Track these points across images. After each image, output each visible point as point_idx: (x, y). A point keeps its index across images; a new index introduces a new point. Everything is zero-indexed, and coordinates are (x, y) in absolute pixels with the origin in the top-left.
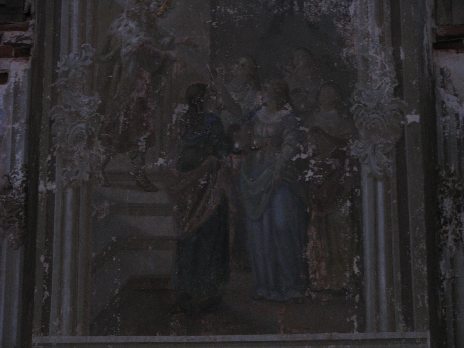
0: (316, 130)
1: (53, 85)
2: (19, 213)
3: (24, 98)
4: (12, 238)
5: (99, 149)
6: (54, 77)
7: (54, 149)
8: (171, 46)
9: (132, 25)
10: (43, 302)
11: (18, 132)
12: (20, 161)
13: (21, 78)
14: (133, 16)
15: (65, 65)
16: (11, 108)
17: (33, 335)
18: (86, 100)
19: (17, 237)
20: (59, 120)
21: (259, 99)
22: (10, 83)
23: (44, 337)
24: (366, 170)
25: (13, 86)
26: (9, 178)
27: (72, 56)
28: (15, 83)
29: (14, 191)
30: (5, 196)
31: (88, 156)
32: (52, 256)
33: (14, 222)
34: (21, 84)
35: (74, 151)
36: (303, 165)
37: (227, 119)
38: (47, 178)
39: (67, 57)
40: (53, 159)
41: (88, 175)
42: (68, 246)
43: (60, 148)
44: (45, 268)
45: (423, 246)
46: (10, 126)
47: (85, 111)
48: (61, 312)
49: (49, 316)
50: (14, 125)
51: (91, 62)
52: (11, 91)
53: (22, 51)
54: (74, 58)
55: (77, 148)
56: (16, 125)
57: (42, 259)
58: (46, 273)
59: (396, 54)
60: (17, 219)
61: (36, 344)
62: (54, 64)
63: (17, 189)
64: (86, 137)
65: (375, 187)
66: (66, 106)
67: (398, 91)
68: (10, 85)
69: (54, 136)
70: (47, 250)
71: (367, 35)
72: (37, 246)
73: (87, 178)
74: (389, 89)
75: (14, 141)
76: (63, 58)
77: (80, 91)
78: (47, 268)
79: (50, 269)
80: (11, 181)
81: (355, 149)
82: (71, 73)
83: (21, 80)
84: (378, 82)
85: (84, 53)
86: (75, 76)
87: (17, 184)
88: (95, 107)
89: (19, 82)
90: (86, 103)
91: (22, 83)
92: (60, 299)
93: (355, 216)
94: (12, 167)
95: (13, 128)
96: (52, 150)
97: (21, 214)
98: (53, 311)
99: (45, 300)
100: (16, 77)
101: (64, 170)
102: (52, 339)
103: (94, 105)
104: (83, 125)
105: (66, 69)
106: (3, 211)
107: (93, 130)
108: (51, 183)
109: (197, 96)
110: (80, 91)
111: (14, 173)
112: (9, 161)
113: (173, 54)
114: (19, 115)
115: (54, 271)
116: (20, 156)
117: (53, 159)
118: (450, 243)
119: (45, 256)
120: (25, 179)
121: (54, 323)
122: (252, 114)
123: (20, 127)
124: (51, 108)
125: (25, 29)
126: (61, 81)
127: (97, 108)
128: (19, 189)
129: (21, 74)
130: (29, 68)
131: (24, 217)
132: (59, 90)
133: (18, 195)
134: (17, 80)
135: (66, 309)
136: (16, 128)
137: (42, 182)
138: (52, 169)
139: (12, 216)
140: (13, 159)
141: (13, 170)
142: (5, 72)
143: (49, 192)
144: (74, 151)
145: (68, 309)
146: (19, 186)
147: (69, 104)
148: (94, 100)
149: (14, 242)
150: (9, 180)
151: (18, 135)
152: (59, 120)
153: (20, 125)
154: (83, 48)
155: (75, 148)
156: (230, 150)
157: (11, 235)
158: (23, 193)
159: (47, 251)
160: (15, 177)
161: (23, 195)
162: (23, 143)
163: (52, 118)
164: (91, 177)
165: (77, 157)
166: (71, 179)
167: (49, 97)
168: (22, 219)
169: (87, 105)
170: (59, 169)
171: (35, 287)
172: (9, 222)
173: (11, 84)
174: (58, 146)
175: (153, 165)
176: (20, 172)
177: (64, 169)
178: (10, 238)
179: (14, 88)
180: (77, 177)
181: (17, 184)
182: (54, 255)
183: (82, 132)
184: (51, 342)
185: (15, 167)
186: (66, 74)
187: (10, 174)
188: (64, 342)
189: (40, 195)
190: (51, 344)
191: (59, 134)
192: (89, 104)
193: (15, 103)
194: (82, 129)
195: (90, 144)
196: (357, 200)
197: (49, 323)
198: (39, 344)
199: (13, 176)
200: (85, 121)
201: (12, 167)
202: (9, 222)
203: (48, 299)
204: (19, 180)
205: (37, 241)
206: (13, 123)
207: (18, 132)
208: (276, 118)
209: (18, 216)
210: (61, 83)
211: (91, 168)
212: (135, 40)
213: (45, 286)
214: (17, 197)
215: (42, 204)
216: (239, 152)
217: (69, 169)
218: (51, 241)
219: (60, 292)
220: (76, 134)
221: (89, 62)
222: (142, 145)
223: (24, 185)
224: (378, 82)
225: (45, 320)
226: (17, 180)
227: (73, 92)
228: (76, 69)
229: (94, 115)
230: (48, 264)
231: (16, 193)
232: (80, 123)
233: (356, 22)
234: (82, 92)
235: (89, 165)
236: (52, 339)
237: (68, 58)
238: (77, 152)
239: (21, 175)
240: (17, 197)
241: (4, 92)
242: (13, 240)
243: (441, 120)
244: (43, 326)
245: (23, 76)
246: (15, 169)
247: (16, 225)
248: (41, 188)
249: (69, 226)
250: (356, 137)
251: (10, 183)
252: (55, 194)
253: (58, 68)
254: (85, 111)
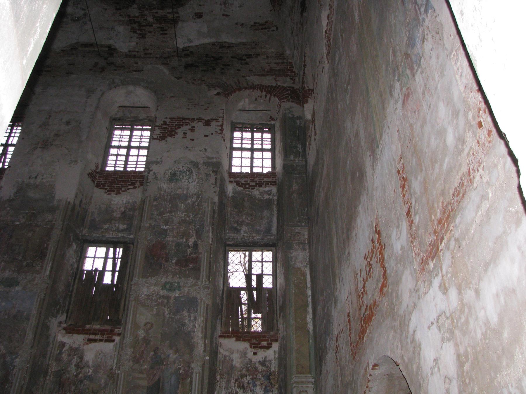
0: (184, 360)
5: (131, 363)
8: (151, 337)
9: (143, 332)
14: (144, 330)
21: (171, 352)
24: (195, 371)
36: (180, 369)
37: (163, 356)
45: (206, 390)
47: (129, 353)
53: (119, 335)
54: (128, 339)
59: (205, 341)
67: (204, 351)
71: (198, 336)
74: (202, 350)
81: (193, 365)
84: (200, 348)
93: (191, 382)
109: (156, 350)
113: (152, 339)
116: (115, 361)
118: (218, 387)
122: (169, 355)
125: (120, 328)
126: (124, 345)
156: (163, 364)
170: (121, 368)
175: (245, 304)
195: (129, 362)
196: (192, 378)
208: (175, 356)
212: (143, 335)
216: (165, 365)
222: (141, 362)
224: (200, 348)
233: (196, 333)
239: (115, 366)
243: (219, 355)
249: (122, 382)
250: (193, 362)
254: (129, 353)
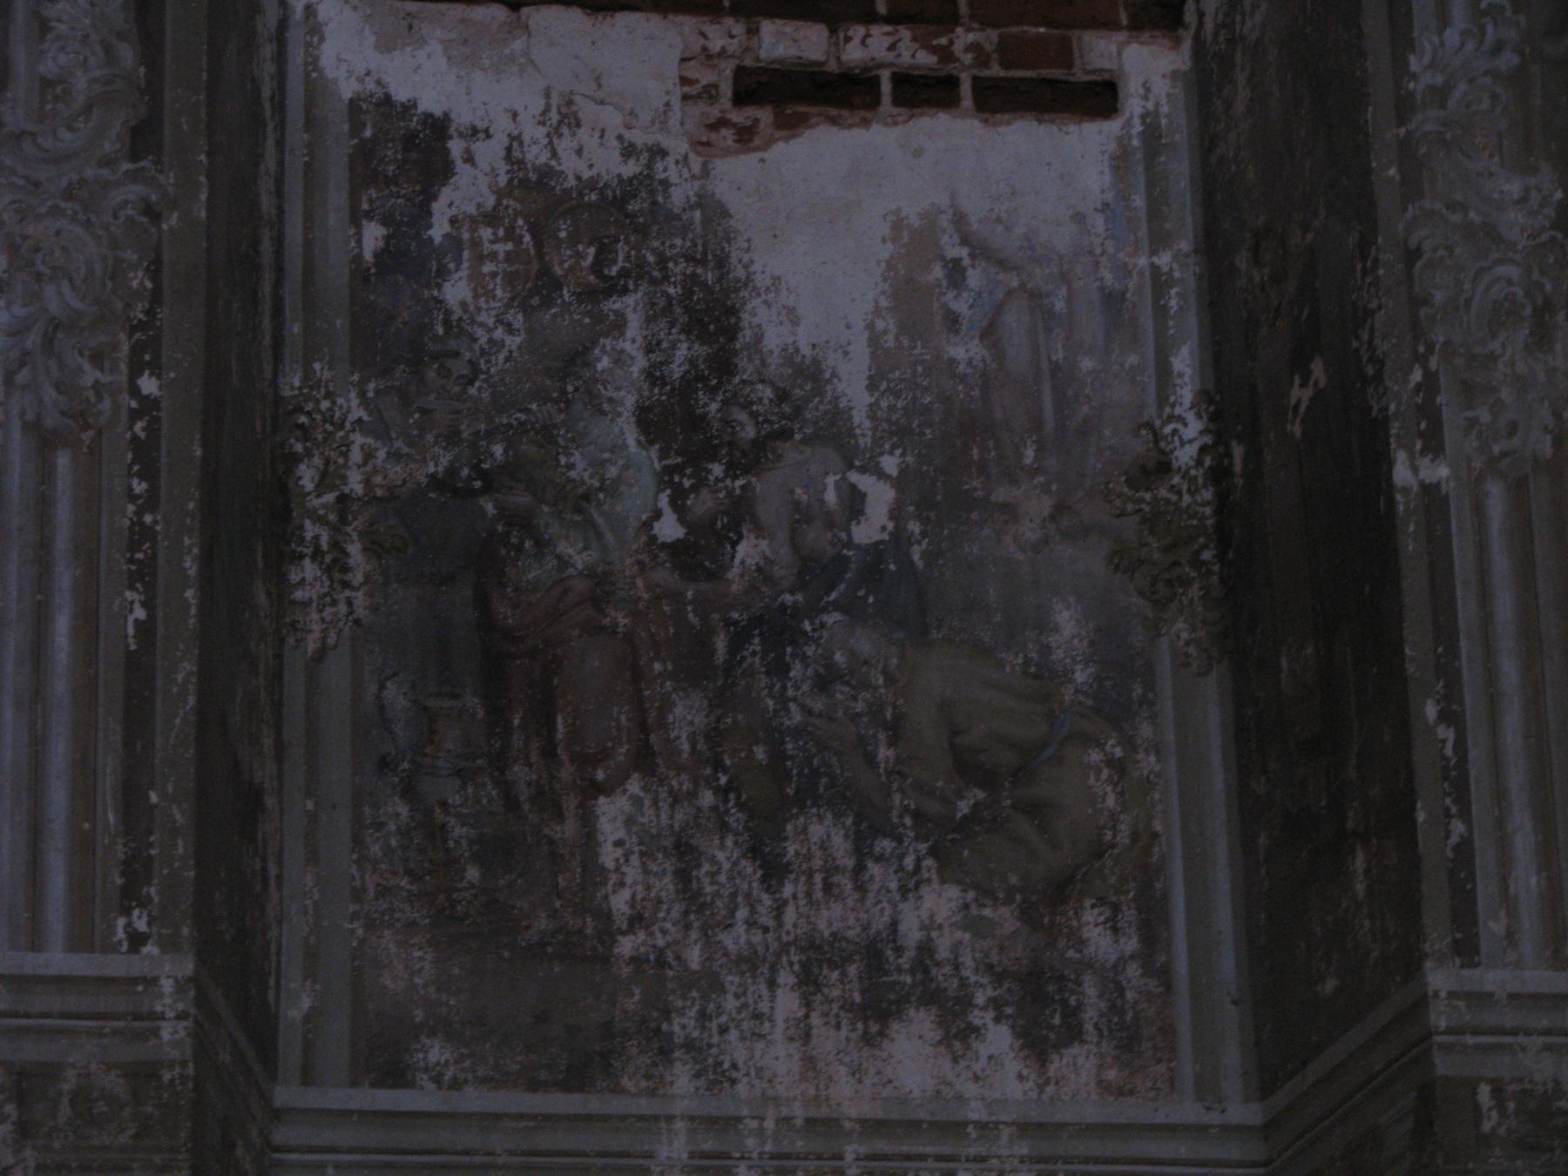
1: (1402, 131)
2: (1198, 553)
3: (1180, 170)
4: (1185, 635)
6: (1404, 108)
7: (1430, 348)
10: (1450, 854)
11: (1171, 283)
12: (1186, 379)
13: (1164, 101)
15: (1432, 65)
16: (1139, 201)
17: (1428, 964)
18: (1514, 187)
19: (1200, 633)
20: (1435, 249)
22: (1127, 114)
23: (1466, 972)
25: (1138, 127)
26: (1157, 436)
27: (1452, 36)
28: (1143, 117)
29: (1176, 480)
30: (1148, 496)
31: (1542, 377)
32: (1461, 703)
33: (1186, 582)
34: (1164, 121)
35: (1493, 357)
38: (1419, 445)
39: (1436, 40)
40: (1430, 380)
41: (1549, 438)
42: (1510, 671)
43: (1447, 343)
44: (1443, 741)
46: (1143, 261)
48: (1512, 890)
49: (1474, 902)
50: (1155, 259)
51: (1516, 60)
52: (1135, 142)
55: (1504, 347)
56: (1164, 260)
57: (1431, 711)
58: (1447, 760)
60: (1194, 574)
61: (1443, 994)
62: (1399, 64)
63: (1187, 472)
64: (1528, 311)
65: (46, 474)
66: (1452, 206)
68: (1128, 124)
69: (1425, 302)
70: (1441, 684)
72: (1411, 669)
73: (1547, 449)
75: (1160, 312)
76: (1426, 44)
77: (1491, 156)
78: (1450, 745)
79: (1460, 744)
80: (1162, 444)
82: (1457, 94)
83: (1165, 109)
85: (1490, 28)
86: (1468, 106)
87: (1185, 456)
88: (1545, 211)
89: (1156, 114)
90: (1515, 197)
91: (1166, 116)
92: (1503, 845)
94: (1162, 400)
95: (1155, 269)
96: (1421, 349)
97: (1206, 555)
98: (1485, 889)
99: (1457, 848)
100: (1146, 98)
101: (1469, 419)
102: (1492, 979)
103: (1541, 206)
104: (1513, 271)
105: (1439, 80)
106: (1146, 545)
107: (1548, 288)
108: (1433, 461)
110: (1491, 156)
111: (1171, 418)
112: (1149, 378)
114: (1167, 226)
115: (1473, 753)
117: (1430, 380)
119: (1438, 702)
120: (1208, 439)
121: (1493, 926)
123: (1175, 266)
124: (1405, 210)
126: (1426, 120)
127: (1553, 214)
128: (1193, 472)
129: (1161, 87)
130: (1185, 68)
131: (1216, 568)
132: (1423, 150)
133: (1189, 490)
134: (1150, 106)
135: (1527, 881)
136: (1165, 269)
137: (1401, 457)
138: (1429, 412)
139: (1176, 563)
140: (1164, 372)
141: (1168, 410)
142: (1106, 76)
143: (1430, 491)
144: (1493, 357)
145: (1533, 880)
146: (1192, 463)
147: (1459, 197)
148: (1539, 190)
149: (1191, 650)
150: (1156, 442)
151: (1173, 292)
152: (1435, 249)
153: (1175, 257)
154: (1484, 13)
155: (1495, 346)
157: (1180, 625)
158: (1205, 485)
159: (1445, 686)
160: (1175, 432)
161: (1208, 494)
162: (1192, 321)
163: (1413, 244)
164: (1557, 443)
165: (1505, 375)
166: (1496, 449)
167: (1392, 171)
168: (1209, 572)
169: (1517, 202)
171: (1419, 805)
172: (1169, 583)
173: (1131, 118)
174: (1441, 339)
176: (1190, 417)
177: (1470, 414)
178: (1178, 637)
179: (1143, 132)
180: (1515, 442)
181: (1185, 456)
182: (1467, 698)
183: (1514, 295)
184: (1489, 988)
185: (1172, 399)
186: (1440, 95)
187: (1158, 422)
188: (1531, 989)
189: (1399, 497)
190: (1491, 995)
191: (1439, 297)
192: (1523, 200)
193: (1150, 184)
194: (1510, 282)
197: (1475, 923)
198: (1452, 995)
199: (1168, 429)
200: (1518, 257)
201: (1162, 400)
202: (1169, 583)
203: (1465, 849)
204: (1191, 441)
205: (1407, 651)
206: (1154, 252)
207: (1171, 283)
209: (1196, 562)
210: (1428, 127)
211: (1557, 415)
213: (1448, 801)
214: (1187, 498)
215: (1411, 529)
217: (1485, 416)
218: (1453, 651)
219: (1500, 824)
220: (1495, 301)
221: (1508, 60)
223: (1208, 462)
225: (1464, 913)
226: (1183, 443)
227: (1469, 157)
228: (1471, 81)
229: (1544, 238)
230: (1452, 730)
231: (1185, 487)
232: (1501, 262)
234: (1496, 159)
235: (1546, 404)
236: (1492, 979)
237: (1442, 44)
238: (1506, 358)
239: (1193, 428)
240: (1187, 498)
241: (1112, 147)
242: (1187, 644)
244: (1459, 936)
245: (1168, 96)
246: (1173, 406)
247: (1195, 591)
248: (1402, 474)
251: (1162, 452)
252: (1447, 496)
253: (1414, 77)
254: (1514, 223)
